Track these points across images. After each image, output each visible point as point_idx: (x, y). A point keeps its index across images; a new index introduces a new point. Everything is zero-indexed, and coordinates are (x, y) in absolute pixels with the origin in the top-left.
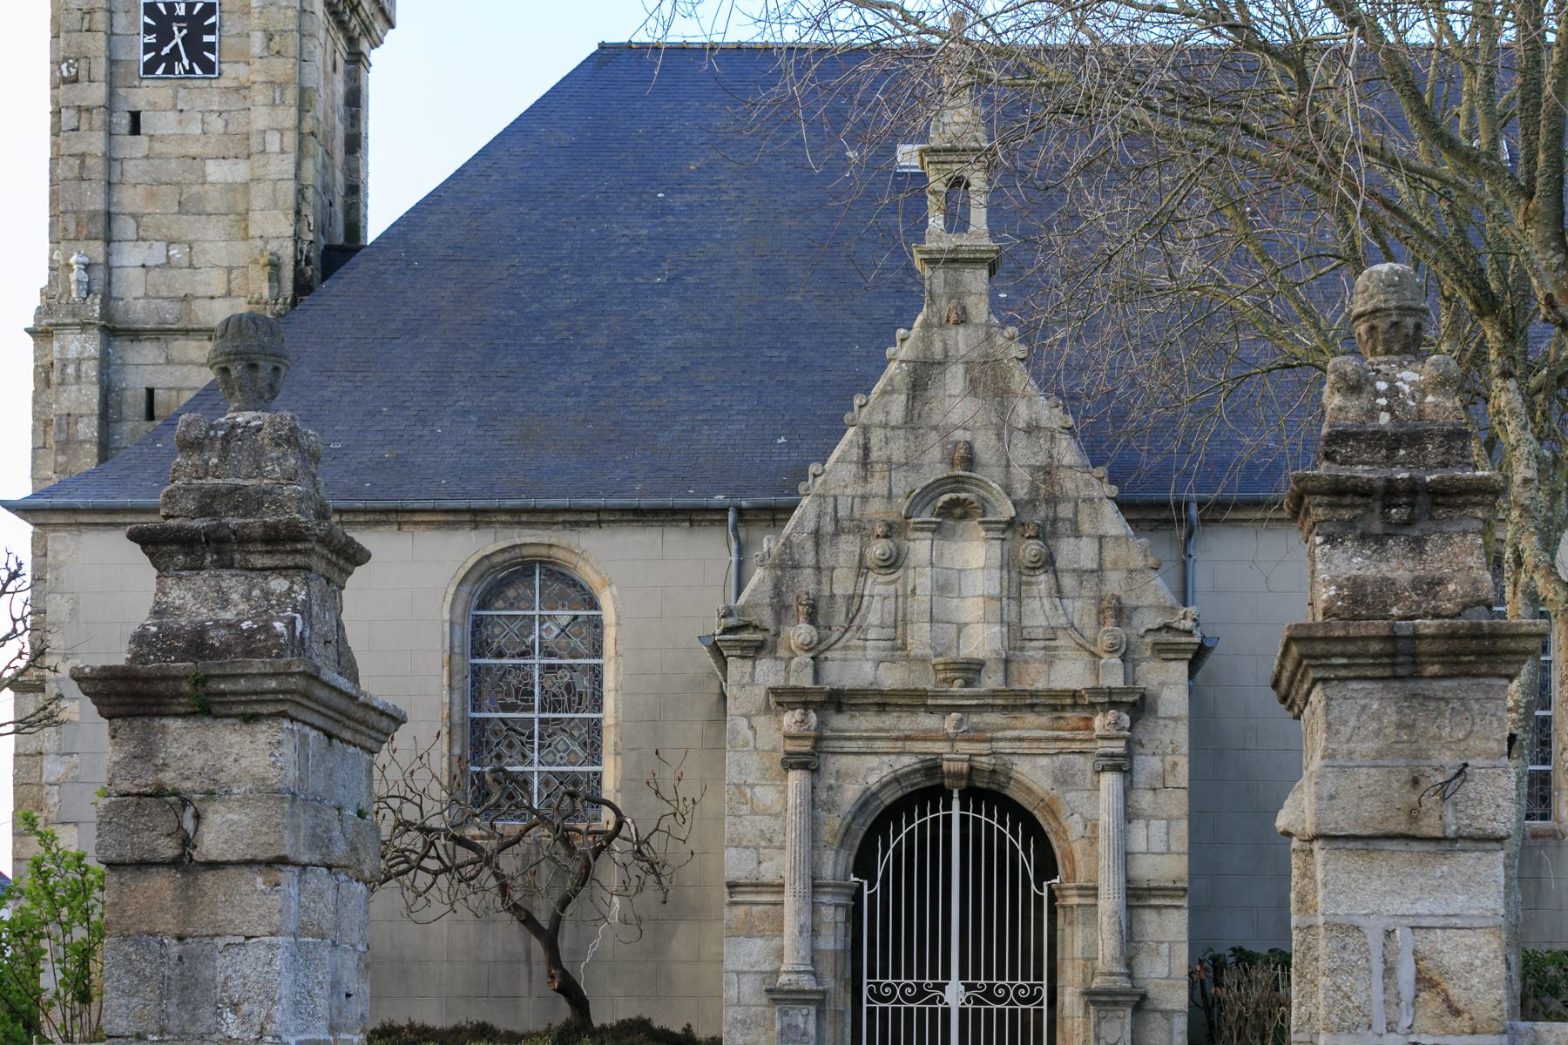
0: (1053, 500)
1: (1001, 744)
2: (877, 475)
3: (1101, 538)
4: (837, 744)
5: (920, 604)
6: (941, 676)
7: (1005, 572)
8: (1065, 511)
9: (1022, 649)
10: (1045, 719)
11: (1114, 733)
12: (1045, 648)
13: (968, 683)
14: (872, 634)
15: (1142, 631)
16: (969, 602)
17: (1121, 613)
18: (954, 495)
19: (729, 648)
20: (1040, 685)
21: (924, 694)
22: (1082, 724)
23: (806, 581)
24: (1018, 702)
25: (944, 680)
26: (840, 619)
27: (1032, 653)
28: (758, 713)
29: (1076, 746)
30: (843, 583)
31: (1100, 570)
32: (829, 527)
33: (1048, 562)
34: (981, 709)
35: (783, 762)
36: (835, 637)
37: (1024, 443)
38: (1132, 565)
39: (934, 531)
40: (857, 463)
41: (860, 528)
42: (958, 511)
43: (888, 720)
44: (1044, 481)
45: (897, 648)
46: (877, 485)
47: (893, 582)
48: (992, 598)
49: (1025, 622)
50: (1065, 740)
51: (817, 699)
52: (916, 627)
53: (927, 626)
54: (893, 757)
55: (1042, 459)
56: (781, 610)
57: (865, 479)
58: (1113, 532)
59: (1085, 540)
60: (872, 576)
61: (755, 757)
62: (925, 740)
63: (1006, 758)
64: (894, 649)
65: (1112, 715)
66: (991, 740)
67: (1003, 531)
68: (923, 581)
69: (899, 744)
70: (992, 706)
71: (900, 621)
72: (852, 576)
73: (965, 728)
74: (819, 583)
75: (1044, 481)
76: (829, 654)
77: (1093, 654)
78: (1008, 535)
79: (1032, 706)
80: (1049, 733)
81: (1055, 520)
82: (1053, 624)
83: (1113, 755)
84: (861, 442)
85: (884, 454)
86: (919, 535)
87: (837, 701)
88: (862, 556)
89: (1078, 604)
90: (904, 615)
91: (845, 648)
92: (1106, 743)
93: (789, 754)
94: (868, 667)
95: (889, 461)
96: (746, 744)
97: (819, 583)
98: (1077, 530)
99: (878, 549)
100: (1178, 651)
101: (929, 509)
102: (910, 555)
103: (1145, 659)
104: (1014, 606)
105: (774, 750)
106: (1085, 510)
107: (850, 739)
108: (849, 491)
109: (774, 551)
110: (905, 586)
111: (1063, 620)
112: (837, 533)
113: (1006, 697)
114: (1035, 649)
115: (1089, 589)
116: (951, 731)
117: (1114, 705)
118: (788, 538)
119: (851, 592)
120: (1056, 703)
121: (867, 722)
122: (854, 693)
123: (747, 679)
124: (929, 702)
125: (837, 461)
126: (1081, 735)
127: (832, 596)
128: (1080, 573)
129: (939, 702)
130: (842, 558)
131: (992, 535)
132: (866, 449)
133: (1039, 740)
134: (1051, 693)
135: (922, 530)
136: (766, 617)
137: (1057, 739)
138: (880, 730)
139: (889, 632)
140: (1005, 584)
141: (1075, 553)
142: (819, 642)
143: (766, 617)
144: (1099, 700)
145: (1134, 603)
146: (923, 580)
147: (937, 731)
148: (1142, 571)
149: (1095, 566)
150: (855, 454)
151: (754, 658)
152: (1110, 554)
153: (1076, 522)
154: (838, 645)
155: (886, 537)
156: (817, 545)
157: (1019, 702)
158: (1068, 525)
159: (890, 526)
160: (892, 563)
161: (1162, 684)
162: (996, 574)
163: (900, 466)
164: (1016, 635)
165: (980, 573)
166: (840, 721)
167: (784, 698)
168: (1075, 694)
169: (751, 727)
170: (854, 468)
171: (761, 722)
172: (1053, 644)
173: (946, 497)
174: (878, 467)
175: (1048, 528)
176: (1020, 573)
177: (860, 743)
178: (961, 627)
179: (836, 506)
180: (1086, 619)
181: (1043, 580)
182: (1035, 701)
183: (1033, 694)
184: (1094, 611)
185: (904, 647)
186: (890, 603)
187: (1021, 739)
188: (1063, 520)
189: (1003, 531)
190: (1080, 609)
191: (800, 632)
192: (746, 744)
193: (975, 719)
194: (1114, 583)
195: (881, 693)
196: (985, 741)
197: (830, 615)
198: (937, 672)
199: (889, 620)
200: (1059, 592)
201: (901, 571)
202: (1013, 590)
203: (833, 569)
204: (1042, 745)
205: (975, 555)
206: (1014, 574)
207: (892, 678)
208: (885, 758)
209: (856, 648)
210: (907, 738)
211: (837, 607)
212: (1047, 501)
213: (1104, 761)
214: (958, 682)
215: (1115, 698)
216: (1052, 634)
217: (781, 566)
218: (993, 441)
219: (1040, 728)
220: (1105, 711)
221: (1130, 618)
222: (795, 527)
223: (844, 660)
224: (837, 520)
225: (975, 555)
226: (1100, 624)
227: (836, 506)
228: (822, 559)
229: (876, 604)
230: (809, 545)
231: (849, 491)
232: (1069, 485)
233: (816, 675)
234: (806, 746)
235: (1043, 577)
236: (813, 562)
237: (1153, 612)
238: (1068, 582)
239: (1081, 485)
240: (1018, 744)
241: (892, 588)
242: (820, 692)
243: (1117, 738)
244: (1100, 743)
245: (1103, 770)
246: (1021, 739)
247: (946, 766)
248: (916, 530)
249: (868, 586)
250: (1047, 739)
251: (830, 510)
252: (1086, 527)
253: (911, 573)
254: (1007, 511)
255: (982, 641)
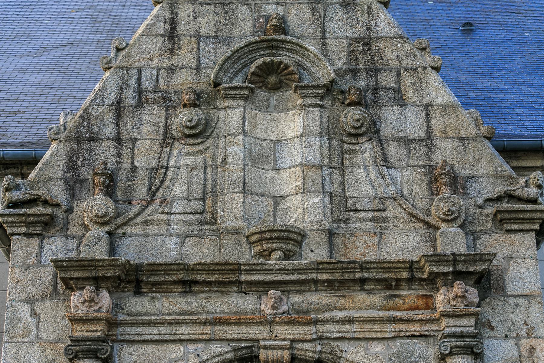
0: (374, 70)
1: (328, 327)
2: (185, 47)
3: (427, 107)
4: (134, 330)
5: (234, 172)
6: (256, 249)
7: (325, 140)
8: (387, 80)
9: (347, 221)
10: (377, 298)
11: (461, 308)
12: (373, 220)
13: (287, 256)
14: (177, 207)
15: (480, 201)
16: (286, 174)
17: (458, 183)
18: (268, 59)
19: (13, 224)
20: (372, 256)
21: (235, 268)
22: (421, 302)
23: (105, 152)
24: (347, 276)
25: (260, 254)
26: (142, 191)
27: (357, 225)
28: (44, 298)
29: (416, 328)
30: (145, 155)
31: (428, 139)
32: (131, 99)
33: (371, 130)
34: (302, 286)
35: (67, 350)
36: (135, 210)
37: (340, 16)
38: (463, 133)
39: (246, 98)
40: (163, 36)
41: (167, 100)
42: (273, 79)
43: (194, 302)
44: (364, 52)
45: (206, 222)
46: (185, 56)
47: (202, 152)
48: (312, 166)
49: (350, 192)
50: (402, 320)
51: (110, 273)
52: (227, 198)
53: (239, 198)
54: (201, 345)
55: (359, 31)
56: (75, 185)
57: (172, 52)
58: (440, 100)
59: (409, 110)
60: (177, 147)
61: (37, 348)
62: (238, 323)
63: (334, 344)
64: (202, 223)
65: (458, 287)
66: (316, 322)
67: (322, 98)
68: (236, 152)
69: (208, 329)
70: (316, 282)
71: (210, 194)
72: (156, 147)
73: (284, 308)
74: (119, 155)
75: (364, 52)
76: (128, 230)
77: (428, 225)
78: (327, 102)
79: (363, 281)
80: (382, 314)
81: (376, 89)
82: (381, 194)
83: (462, 336)
84: (168, 15)
85: (192, 28)
86: (230, 103)
87: (134, 279)
88: (167, 127)
89: (407, 173)
90: (214, 186)
91: (146, 222)
92: (452, 322)
93: (76, 340)
94: (172, 243)
95: (197, 35)
96: (27, 334)
97: (119, 155)
98: (401, 98)
99: (184, 116)
100: (524, 220)
101: (240, 77)
102: (221, 124)
103: (485, 232)
104: (336, 175)
105: (60, 340)
106: (408, 79)
107: (149, 324)
108: (154, 63)
109: (70, 125)
110: (214, 156)
111: (391, 190)
112: (139, 105)
113: (333, 271)
114: (362, 220)
115: (418, 158)
116: (268, 311)
117: (459, 275)
118: (86, 110)
119: (154, 164)
120: (390, 278)
121: (169, 304)
122: (155, 268)
123: (32, 259)
124: (243, 278)
125: (142, 35)
126: (421, 315)
127: (133, 169)
128: (407, 142)
129: (254, 278)
130: (145, 130)
131: (309, 101)
132: (173, 23)
133: (371, 321)
134: (385, 265)
135: (233, 97)
136: (58, 192)
137: (393, 320)
138: (186, 313)
139: (197, 205)
140: (326, 153)
141: (401, 121)
142: (117, 215)
143: (58, 192)
144: (442, 269)
145: (468, 171)
146: (234, 148)
147: (253, 312)
148: (474, 139)
149: (423, 135)
150: (161, 27)
151: (41, 236)
152: (439, 123)
153: (400, 91)
154: (139, 219)
155: (195, 105)
156: (118, 117)
157: (346, 277)
158: (391, 93)
159: (199, 96)
160: (199, 133)
161: (509, 258)
162: (315, 141)
163: (208, 38)
164: (341, 207)
165: (297, 141)
166: (137, 304)
167: (73, 275)
168: (411, 266)
169: (34, 314)
170: (160, 41)
171: (46, 308)
172: (382, 215)
173: (259, 62)
174: (185, 40)
175: (370, 96)
176: (342, 142)
177: (162, 329)
178: (278, 200)
179: (139, 79)
180: (416, 190)
181: (367, 150)
182: (366, 275)
183: (363, 266)
184: (425, 181)
185: (213, 221)
186: (198, 175)
187: (350, 321)
188: (385, 88)
189: (322, 98)
190: (410, 179)
191: (95, 203)
192: (27, 334)
193: (296, 298)
194: (446, 150)
195: (187, 268)
196: (309, 323)
197: (130, 188)
198: (251, 244)
199: (197, 191)
200: (385, 161)
201: (211, 140)
202: (335, 158)
203: (135, 140)
204: (376, 327)
205: (293, 126)
206: (335, 143)
207: (200, 252)
208: (191, 347)
209: (159, 222)
210: (218, 322)
211: (138, 180)
212: (367, 71)
213: (452, 342)
214: (277, 254)
215: (461, 268)
216: (380, 205)
217: (78, 139)
218: (307, 15)
219: (372, 307)
220: (449, 285)
221: (465, 188)
222: (95, 99)
223: (146, 236)
224: (140, 92)
225: (293, 126)
226: (433, 194)
227: (139, 79)
228: (123, 131)
229: (183, 176)
230: (109, 117)
231: (154, 63)
232: (390, 55)
233: (112, 250)
234: (97, 330)
235: (367, 145)
236: (113, 134)
237: (491, 181)
238: (395, 151)
239: (403, 55)
240: (347, 327)
241: (200, 159)
242: (114, 264)
243: (466, 315)
244: (445, 322)
245: (451, 354)
246: (350, 321)
247: (263, 354)
248: (226, 97)
249: (174, 158)
250: (382, 321)
251: (133, 81)
252: (410, 95)
253: (221, 143)
254: (325, 73)
255: (303, 211)
